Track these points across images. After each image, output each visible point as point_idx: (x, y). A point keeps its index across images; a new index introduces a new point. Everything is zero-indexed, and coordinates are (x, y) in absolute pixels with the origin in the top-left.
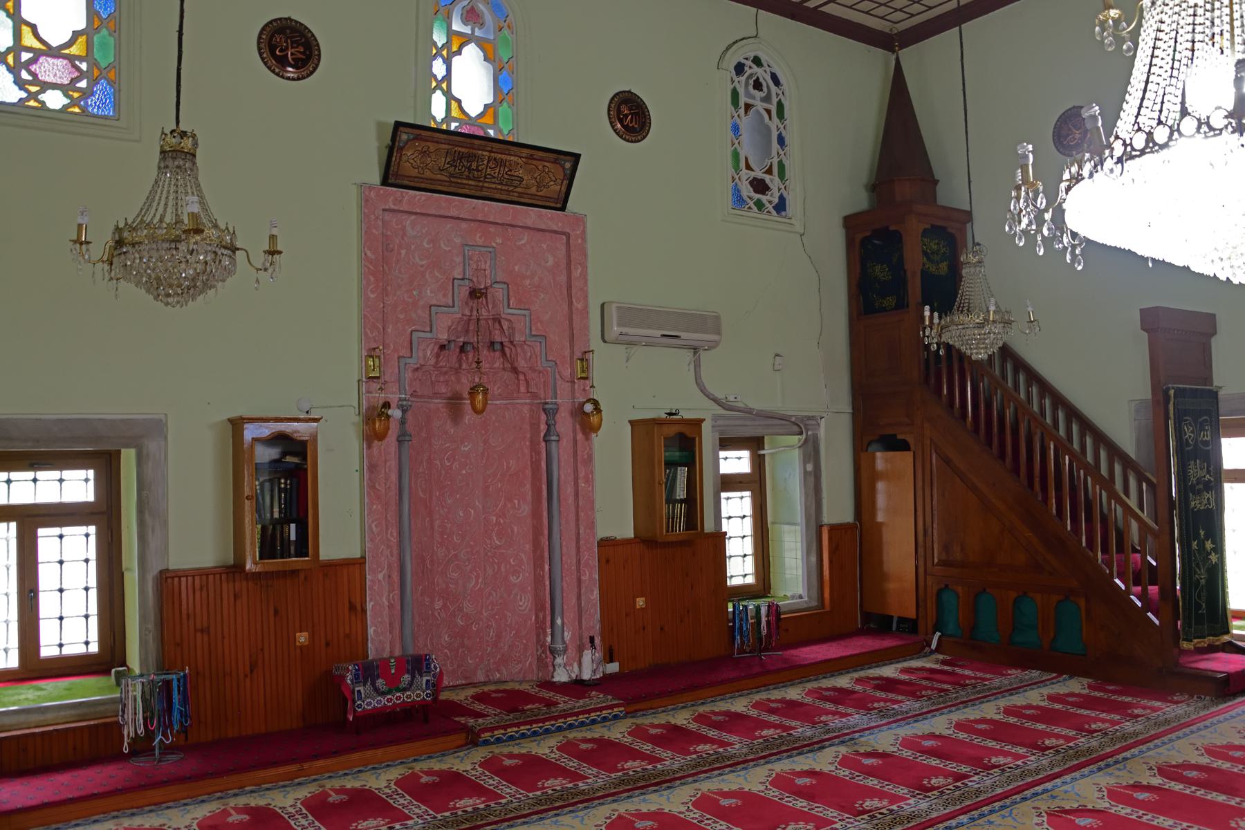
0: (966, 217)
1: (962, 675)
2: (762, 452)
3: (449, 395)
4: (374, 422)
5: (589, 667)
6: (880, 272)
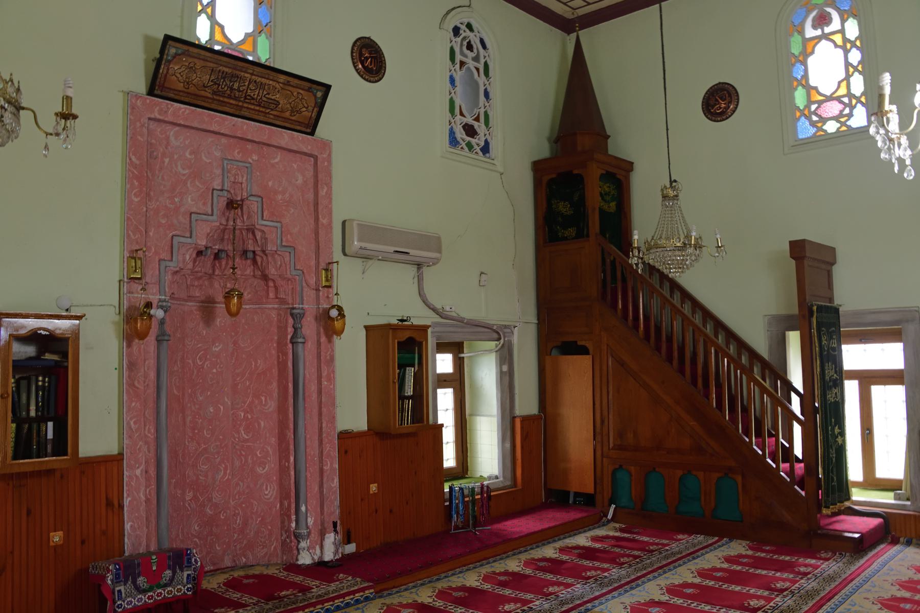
0: (628, 167)
1: (643, 542)
2: (462, 355)
3: (203, 298)
4: (135, 322)
5: (330, 549)
6: (564, 208)
